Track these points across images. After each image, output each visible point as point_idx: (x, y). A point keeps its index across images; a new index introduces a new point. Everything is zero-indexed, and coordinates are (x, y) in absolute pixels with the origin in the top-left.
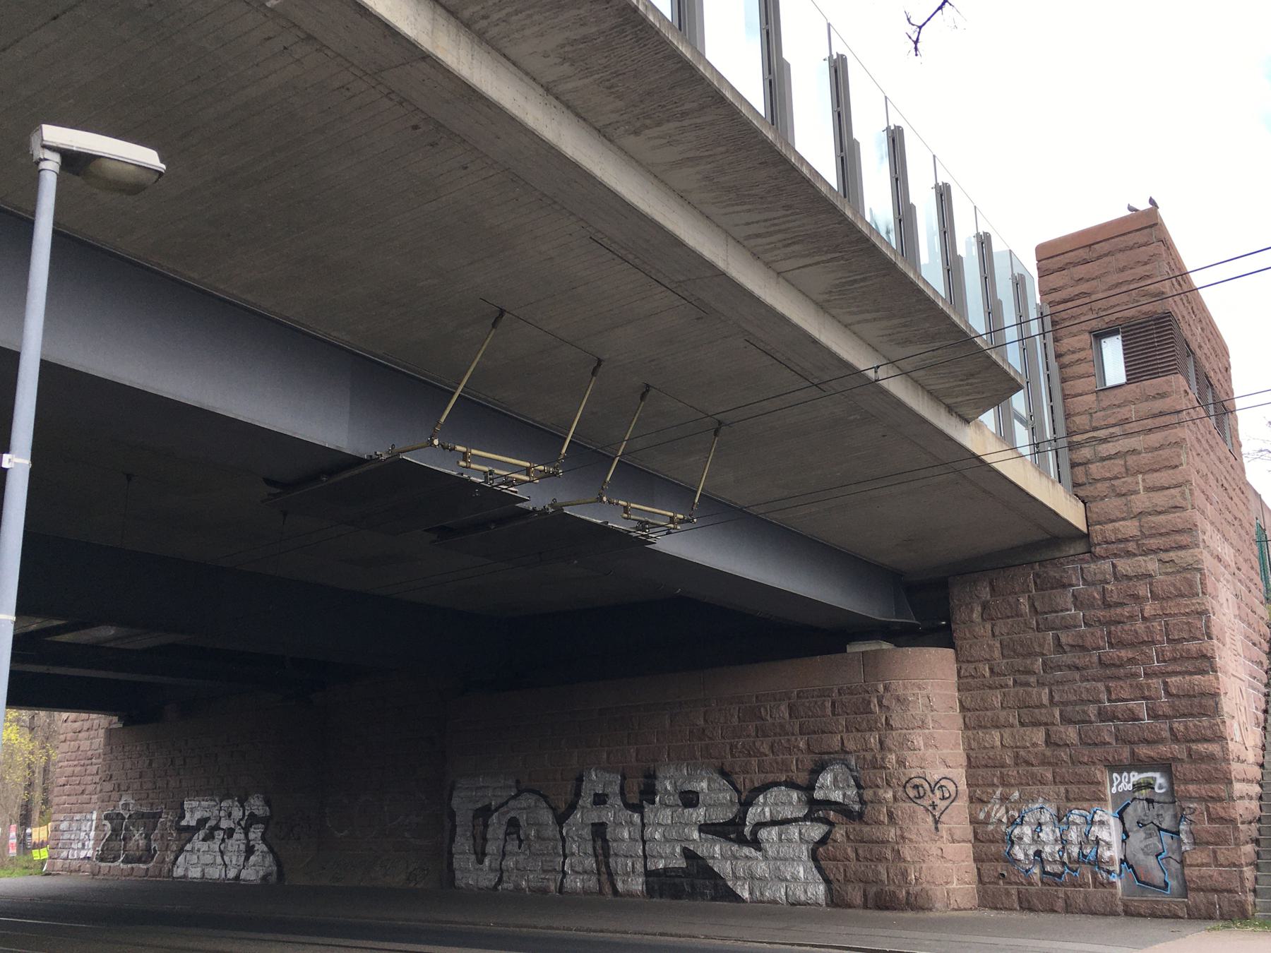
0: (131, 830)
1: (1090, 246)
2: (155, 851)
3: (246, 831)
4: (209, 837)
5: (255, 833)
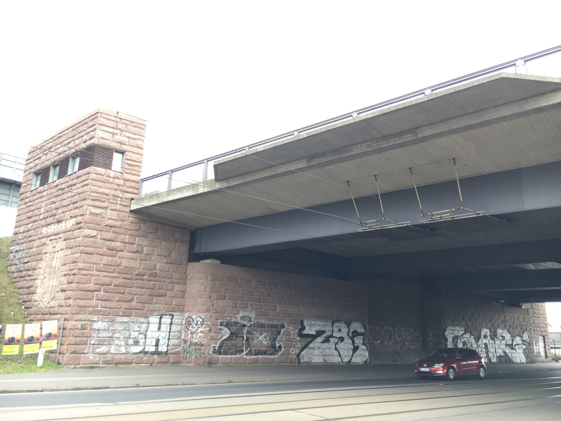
0: (254, 334)
1: (132, 122)
2: (280, 347)
3: (352, 338)
4: (327, 340)
5: (359, 341)
